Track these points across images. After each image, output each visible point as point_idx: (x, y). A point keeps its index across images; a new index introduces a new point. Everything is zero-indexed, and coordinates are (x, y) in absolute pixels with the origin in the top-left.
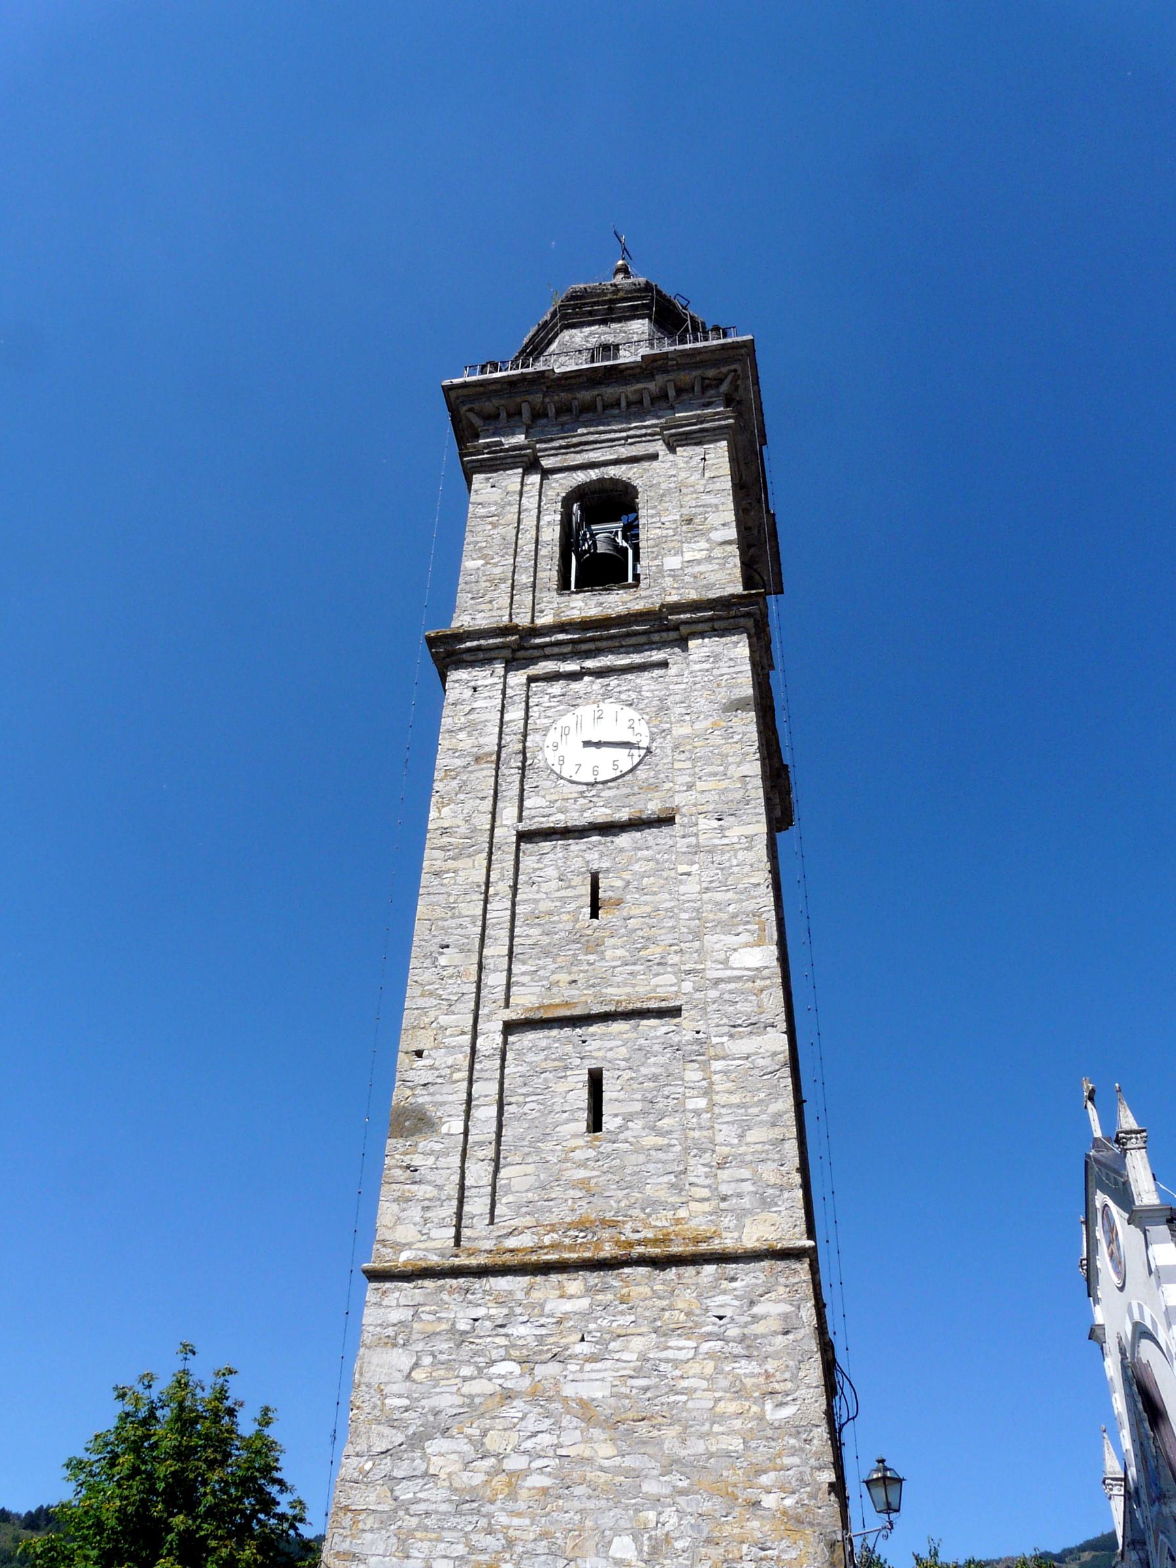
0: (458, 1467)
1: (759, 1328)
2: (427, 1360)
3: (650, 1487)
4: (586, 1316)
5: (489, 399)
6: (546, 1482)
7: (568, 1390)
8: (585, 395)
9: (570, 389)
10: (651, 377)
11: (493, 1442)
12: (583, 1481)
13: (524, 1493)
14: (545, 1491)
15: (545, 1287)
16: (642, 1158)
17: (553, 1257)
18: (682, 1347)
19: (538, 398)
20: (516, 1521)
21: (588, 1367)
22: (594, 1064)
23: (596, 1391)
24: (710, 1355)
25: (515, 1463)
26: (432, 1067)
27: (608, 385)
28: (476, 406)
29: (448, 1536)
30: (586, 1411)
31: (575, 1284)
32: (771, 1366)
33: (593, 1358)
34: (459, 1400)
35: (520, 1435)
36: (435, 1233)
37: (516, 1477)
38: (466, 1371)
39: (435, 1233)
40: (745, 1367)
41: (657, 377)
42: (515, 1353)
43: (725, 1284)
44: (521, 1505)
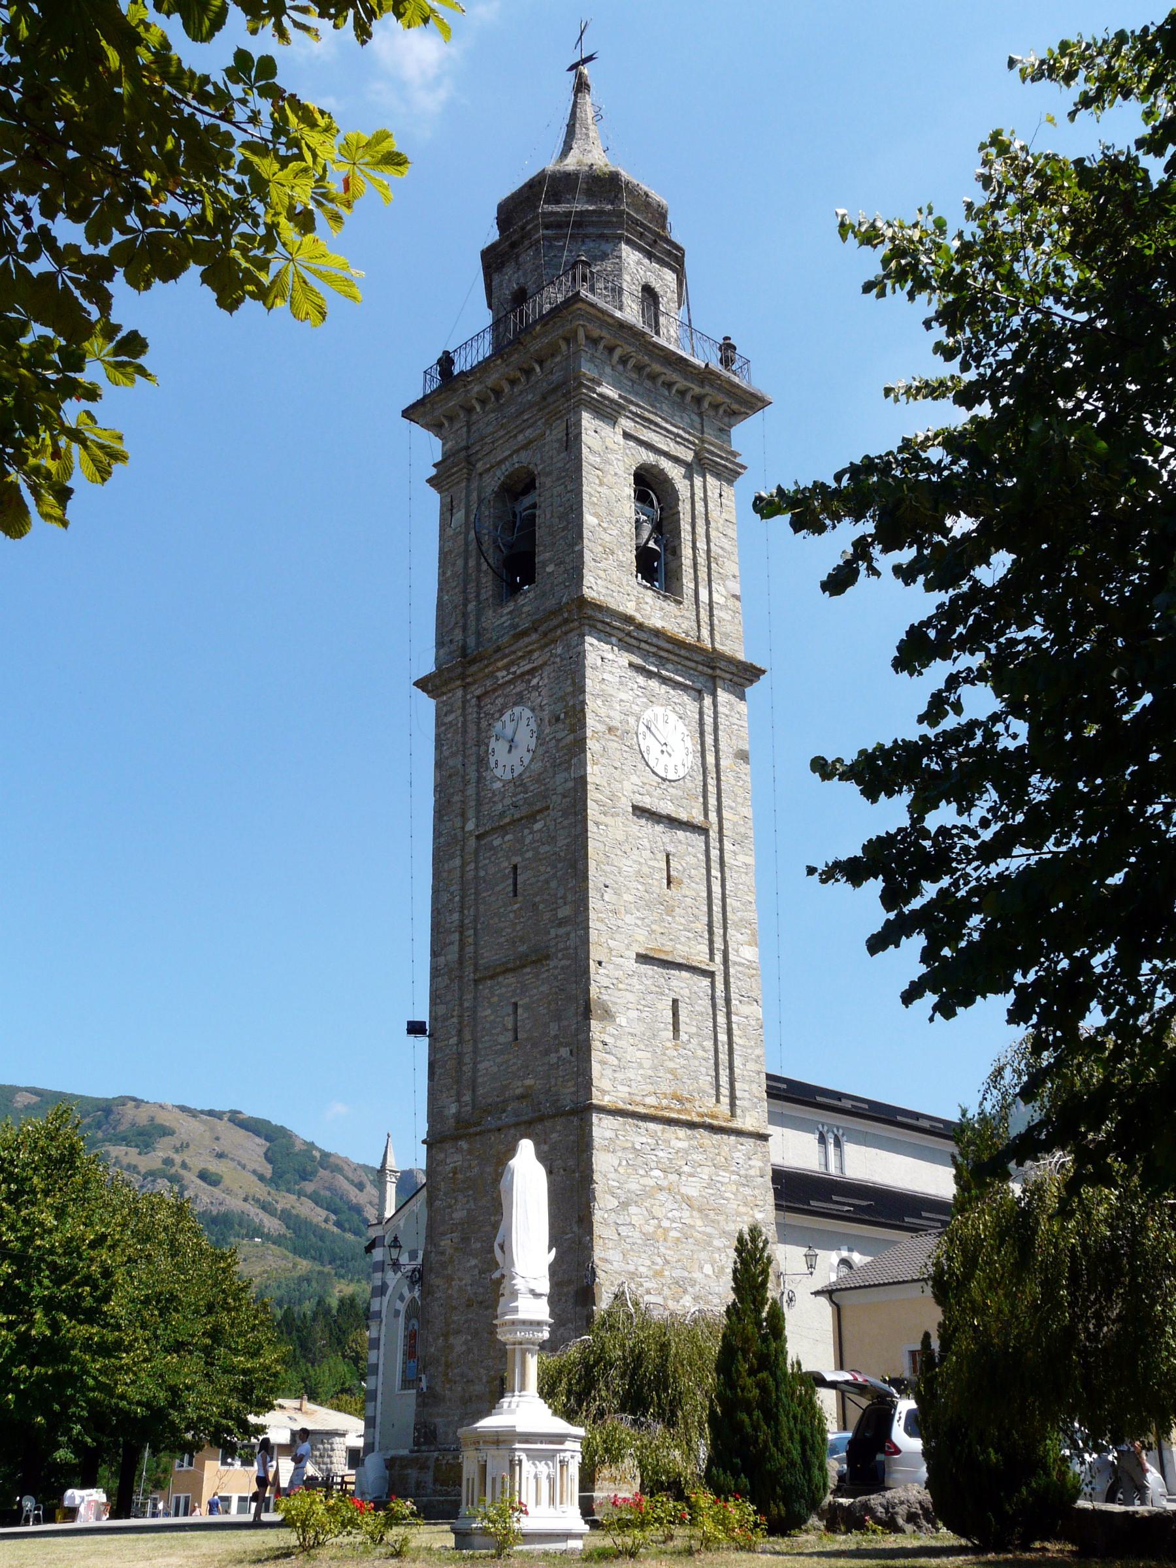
0: (642, 1222)
1: (752, 1172)
2: (624, 1163)
3: (716, 1243)
4: (686, 1151)
5: (600, 327)
6: (678, 1235)
7: (683, 1190)
8: (657, 367)
9: (651, 354)
10: (702, 384)
11: (657, 1211)
12: (692, 1237)
13: (670, 1239)
14: (678, 1239)
15: (671, 1132)
16: (697, 1063)
17: (674, 1115)
18: (724, 1176)
19: (630, 349)
20: (668, 1252)
21: (690, 1179)
22: (673, 995)
23: (693, 1192)
24: (735, 1182)
25: (666, 1224)
26: (607, 976)
27: (675, 370)
28: (589, 326)
29: (643, 1256)
30: (688, 1201)
31: (682, 1132)
32: (756, 1192)
33: (691, 1175)
34: (638, 1187)
35: (664, 1206)
36: (620, 1088)
37: (666, 1230)
38: (642, 1172)
39: (620, 1088)
40: (747, 1191)
41: (994, 559)
42: (660, 1166)
43: (740, 1147)
44: (669, 1244)
